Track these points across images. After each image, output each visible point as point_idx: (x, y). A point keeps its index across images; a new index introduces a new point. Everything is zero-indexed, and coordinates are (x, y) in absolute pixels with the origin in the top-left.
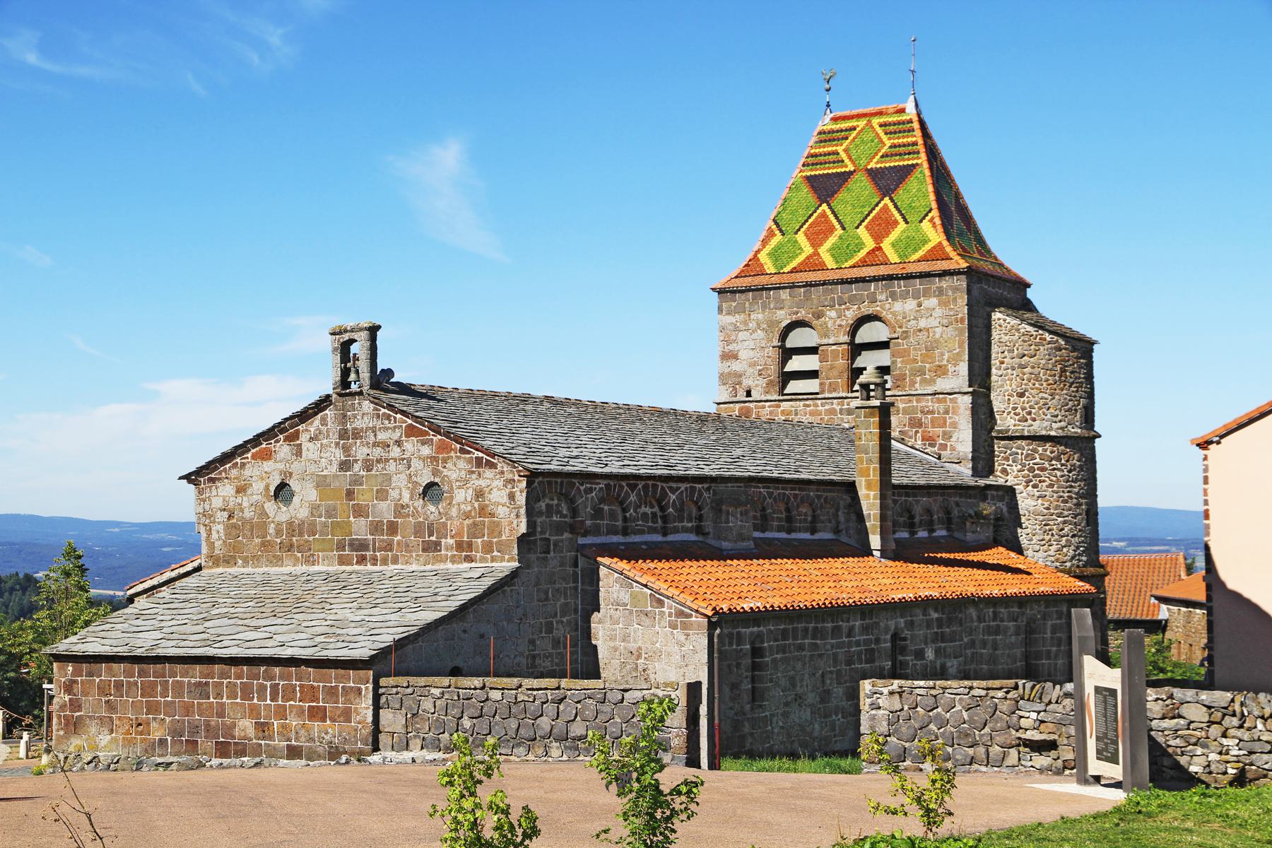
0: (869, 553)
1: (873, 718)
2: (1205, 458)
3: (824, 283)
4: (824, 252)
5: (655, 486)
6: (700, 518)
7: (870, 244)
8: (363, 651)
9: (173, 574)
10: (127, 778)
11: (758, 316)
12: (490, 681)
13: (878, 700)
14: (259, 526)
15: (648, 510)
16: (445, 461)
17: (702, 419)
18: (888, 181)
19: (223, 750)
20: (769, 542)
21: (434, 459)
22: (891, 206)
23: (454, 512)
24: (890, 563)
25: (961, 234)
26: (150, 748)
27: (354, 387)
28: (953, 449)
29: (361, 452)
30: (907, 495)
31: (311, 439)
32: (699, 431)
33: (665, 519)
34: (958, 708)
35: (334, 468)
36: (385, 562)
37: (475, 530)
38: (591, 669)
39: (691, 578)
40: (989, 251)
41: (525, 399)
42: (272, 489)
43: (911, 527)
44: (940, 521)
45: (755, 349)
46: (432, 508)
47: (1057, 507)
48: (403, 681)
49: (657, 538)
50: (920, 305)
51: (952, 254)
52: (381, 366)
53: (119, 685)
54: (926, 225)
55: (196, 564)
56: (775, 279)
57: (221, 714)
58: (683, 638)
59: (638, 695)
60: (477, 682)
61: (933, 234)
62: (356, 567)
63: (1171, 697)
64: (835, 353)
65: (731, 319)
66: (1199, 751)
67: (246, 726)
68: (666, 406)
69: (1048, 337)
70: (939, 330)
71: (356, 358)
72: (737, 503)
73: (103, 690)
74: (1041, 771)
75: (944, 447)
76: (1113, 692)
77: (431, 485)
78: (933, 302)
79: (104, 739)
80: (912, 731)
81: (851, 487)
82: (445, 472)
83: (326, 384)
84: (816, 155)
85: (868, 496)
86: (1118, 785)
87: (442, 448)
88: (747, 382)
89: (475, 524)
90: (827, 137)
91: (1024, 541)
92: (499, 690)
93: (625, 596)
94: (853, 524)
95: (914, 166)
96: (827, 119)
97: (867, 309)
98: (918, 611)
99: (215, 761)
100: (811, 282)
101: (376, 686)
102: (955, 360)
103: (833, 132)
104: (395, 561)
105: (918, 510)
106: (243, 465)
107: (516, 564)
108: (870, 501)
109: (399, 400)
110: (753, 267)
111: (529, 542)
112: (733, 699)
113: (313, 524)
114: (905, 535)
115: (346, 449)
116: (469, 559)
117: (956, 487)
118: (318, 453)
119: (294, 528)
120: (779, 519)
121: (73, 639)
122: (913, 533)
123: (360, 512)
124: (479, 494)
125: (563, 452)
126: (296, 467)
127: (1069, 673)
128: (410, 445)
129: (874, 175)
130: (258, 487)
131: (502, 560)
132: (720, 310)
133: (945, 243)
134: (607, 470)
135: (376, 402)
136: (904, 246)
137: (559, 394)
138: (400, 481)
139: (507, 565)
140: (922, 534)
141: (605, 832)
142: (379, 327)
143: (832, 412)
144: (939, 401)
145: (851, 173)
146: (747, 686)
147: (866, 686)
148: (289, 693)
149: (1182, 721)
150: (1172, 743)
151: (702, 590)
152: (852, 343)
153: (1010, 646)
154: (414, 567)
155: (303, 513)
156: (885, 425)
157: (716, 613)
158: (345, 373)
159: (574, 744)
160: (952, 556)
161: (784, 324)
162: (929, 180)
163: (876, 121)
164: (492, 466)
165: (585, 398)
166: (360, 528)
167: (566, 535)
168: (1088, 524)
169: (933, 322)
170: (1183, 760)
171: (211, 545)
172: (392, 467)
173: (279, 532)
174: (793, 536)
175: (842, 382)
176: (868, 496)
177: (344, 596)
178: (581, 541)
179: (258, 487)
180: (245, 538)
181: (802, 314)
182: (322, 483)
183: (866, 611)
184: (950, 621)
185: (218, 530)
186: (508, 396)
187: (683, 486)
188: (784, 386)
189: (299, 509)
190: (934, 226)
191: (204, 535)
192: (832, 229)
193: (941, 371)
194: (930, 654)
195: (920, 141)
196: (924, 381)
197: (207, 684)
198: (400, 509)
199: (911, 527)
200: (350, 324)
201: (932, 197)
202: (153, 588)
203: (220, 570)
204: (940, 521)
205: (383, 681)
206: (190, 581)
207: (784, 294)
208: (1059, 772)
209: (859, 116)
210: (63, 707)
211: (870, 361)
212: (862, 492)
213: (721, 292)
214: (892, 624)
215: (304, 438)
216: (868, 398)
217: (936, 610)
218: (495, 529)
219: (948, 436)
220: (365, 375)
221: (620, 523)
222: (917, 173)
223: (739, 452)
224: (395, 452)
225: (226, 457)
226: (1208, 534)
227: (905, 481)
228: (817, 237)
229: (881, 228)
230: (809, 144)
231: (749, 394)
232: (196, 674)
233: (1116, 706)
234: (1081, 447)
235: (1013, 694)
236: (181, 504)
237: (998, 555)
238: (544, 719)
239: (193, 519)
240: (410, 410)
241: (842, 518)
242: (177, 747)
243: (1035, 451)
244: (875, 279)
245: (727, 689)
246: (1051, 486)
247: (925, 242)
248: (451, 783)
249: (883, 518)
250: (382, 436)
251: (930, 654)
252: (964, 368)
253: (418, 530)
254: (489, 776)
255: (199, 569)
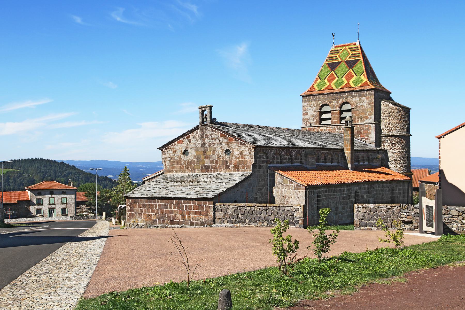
0: (347, 169)
1: (358, 214)
2: (440, 142)
3: (333, 93)
4: (333, 84)
5: (289, 150)
6: (301, 159)
7: (346, 82)
8: (211, 196)
9: (155, 175)
10: (148, 230)
11: (314, 103)
12: (247, 204)
13: (359, 210)
14: (179, 162)
15: (287, 157)
16: (231, 143)
17: (300, 131)
18: (351, 64)
19: (172, 223)
20: (320, 166)
21: (228, 143)
22: (352, 71)
23: (234, 158)
24: (353, 171)
25: (372, 79)
26: (153, 222)
27: (205, 123)
28: (369, 139)
29: (207, 141)
30: (357, 152)
31: (194, 138)
32: (299, 135)
33: (292, 159)
34: (383, 212)
35: (200, 146)
36: (214, 171)
37: (240, 163)
38: (273, 201)
39: (300, 176)
40: (380, 84)
41: (251, 126)
42: (183, 151)
43: (358, 161)
44: (366, 160)
45: (313, 112)
46: (228, 157)
47: (399, 156)
48: (222, 204)
49: (290, 165)
50: (360, 99)
51: (370, 84)
52: (213, 117)
53: (143, 205)
54: (362, 76)
55: (161, 172)
56: (318, 92)
57: (171, 213)
58: (298, 192)
59: (289, 208)
60: (243, 205)
61: (364, 79)
62: (206, 173)
63: (447, 208)
64: (336, 113)
65: (306, 104)
66: (455, 224)
67: (178, 216)
68: (290, 128)
69: (397, 107)
70: (366, 106)
71: (206, 115)
72: (312, 155)
73: (139, 206)
74: (408, 229)
75: (367, 139)
76: (432, 207)
77: (227, 150)
78: (364, 98)
79: (140, 219)
80: (369, 218)
81: (342, 150)
82: (231, 146)
83: (197, 122)
84: (330, 57)
85: (347, 153)
86: (433, 233)
87: (230, 140)
88: (310, 121)
89: (240, 161)
90: (333, 52)
91: (390, 165)
92: (249, 207)
93: (282, 181)
94: (343, 161)
95: (359, 60)
96: (333, 47)
97: (345, 100)
98: (362, 185)
99: (170, 226)
100: (329, 93)
101: (215, 206)
102: (370, 114)
103: (335, 50)
104: (217, 171)
105: (360, 157)
106: (175, 145)
107: (252, 172)
108: (348, 154)
109: (218, 127)
110: (312, 89)
111: (255, 166)
112: (312, 210)
113: (194, 161)
114: (357, 164)
115: (203, 140)
116: (238, 171)
117: (371, 150)
118: (196, 141)
119: (189, 162)
120: (323, 159)
121: (131, 192)
122: (359, 163)
123: (207, 158)
124: (241, 152)
125: (264, 141)
126: (189, 145)
127: (419, 201)
128: (221, 139)
129: (347, 62)
130: (179, 151)
131: (248, 171)
132: (303, 101)
133: (368, 81)
134: (276, 146)
135: (212, 127)
136: (356, 82)
137: (261, 125)
138: (218, 149)
139: (249, 172)
140: (361, 163)
141: (310, 247)
142: (212, 106)
143: (335, 129)
144: (366, 126)
145: (340, 62)
146: (316, 206)
147: (356, 205)
148: (190, 207)
149: (450, 215)
150: (447, 221)
151: (303, 179)
152: (340, 110)
153: (387, 195)
154: (223, 173)
155: (191, 158)
156: (352, 132)
157: (308, 185)
158: (203, 119)
159: (271, 222)
160: (369, 170)
161: (321, 105)
162: (363, 64)
163: (347, 47)
164: (245, 145)
165: (267, 126)
166: (207, 162)
167: (265, 164)
168: (408, 160)
169: (364, 104)
170: (450, 227)
171: (166, 167)
172: (216, 145)
173: (185, 163)
174: (326, 164)
175: (337, 121)
176: (347, 153)
177: (204, 181)
178: (269, 165)
179: (179, 151)
180: (175, 165)
181: (326, 102)
182: (196, 150)
183: (348, 185)
184: (371, 187)
185: (168, 163)
186: (247, 125)
187: (297, 150)
188: (321, 122)
189: (190, 157)
190: (364, 76)
191: (164, 164)
192: (335, 78)
193: (366, 117)
194: (365, 197)
195: (360, 53)
196: (361, 120)
197: (167, 205)
198: (218, 157)
199: (358, 161)
200: (204, 105)
201: (364, 68)
202: (150, 179)
203: (169, 174)
204: (366, 160)
205: (216, 204)
206: (161, 177)
207: (321, 97)
208: (413, 230)
209: (343, 46)
210: (128, 211)
211: (347, 115)
212: (346, 151)
213: (303, 96)
214: (355, 188)
215: (191, 137)
216: (347, 125)
217: (367, 185)
218: (246, 162)
219: (368, 136)
220: (208, 120)
221: (279, 160)
222: (359, 62)
223: (311, 141)
224: (217, 141)
225: (170, 143)
226: (440, 163)
227: (357, 149)
228: (330, 81)
229: (349, 77)
230: (328, 54)
231: (311, 125)
232: (164, 202)
233: (433, 211)
234: (405, 139)
235: (399, 208)
236: (157, 157)
237: (383, 169)
238: (262, 215)
239: (161, 160)
240: (221, 129)
241: (339, 159)
242: (160, 222)
243: (393, 140)
244: (347, 92)
245: (310, 207)
246: (397, 150)
247: (362, 81)
248: (275, 233)
249: (351, 159)
250: (213, 137)
251: (365, 197)
252: (373, 117)
253: (224, 163)
254: (285, 231)
255: (163, 173)
